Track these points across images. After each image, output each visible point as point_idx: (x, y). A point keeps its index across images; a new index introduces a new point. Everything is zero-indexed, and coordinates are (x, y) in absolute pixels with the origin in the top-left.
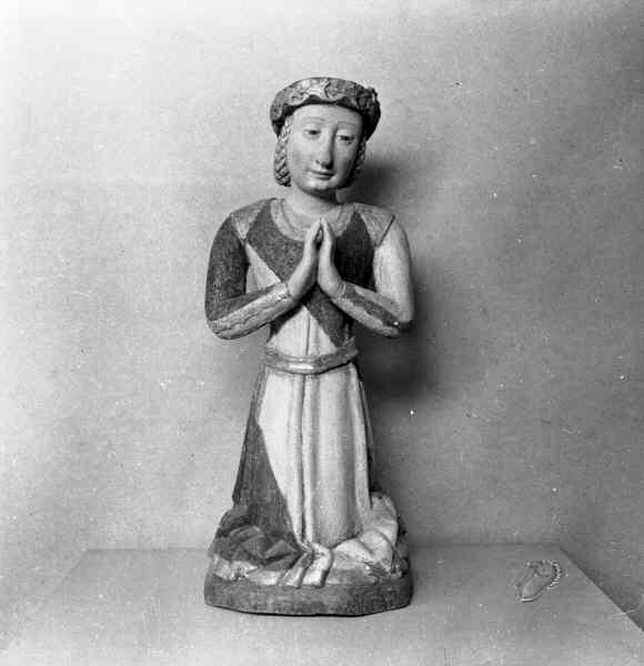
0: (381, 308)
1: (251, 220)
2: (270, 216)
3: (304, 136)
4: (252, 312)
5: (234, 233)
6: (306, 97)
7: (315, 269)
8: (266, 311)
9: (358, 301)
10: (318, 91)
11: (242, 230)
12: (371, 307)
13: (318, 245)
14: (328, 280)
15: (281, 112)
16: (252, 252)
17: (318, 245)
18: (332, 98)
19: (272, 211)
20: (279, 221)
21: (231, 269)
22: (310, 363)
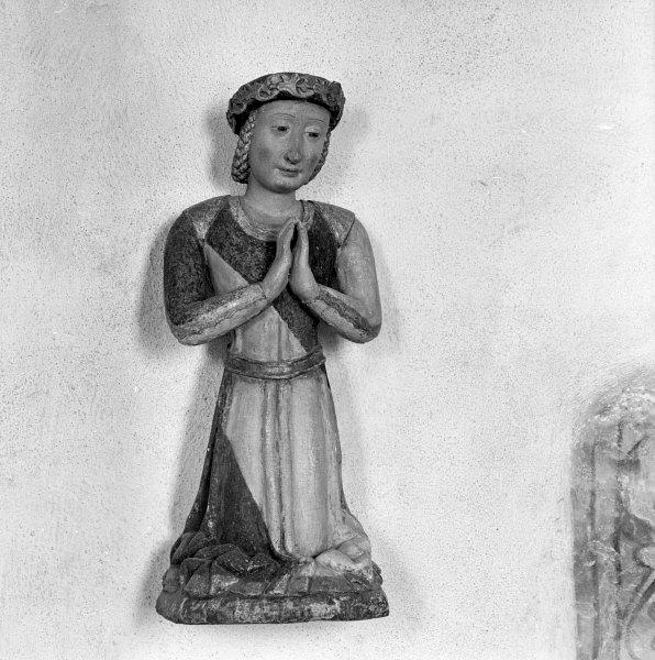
0: (353, 310)
1: (210, 218)
2: (230, 215)
3: (272, 131)
4: (227, 315)
5: (192, 232)
6: (276, 93)
7: (291, 270)
8: (238, 313)
9: (331, 303)
10: (290, 88)
11: (202, 230)
12: (343, 310)
13: (294, 243)
14: (306, 283)
15: (245, 106)
16: (212, 254)
17: (294, 243)
18: (303, 95)
19: (233, 210)
20: (241, 220)
21: (194, 270)
22: (244, 350)
